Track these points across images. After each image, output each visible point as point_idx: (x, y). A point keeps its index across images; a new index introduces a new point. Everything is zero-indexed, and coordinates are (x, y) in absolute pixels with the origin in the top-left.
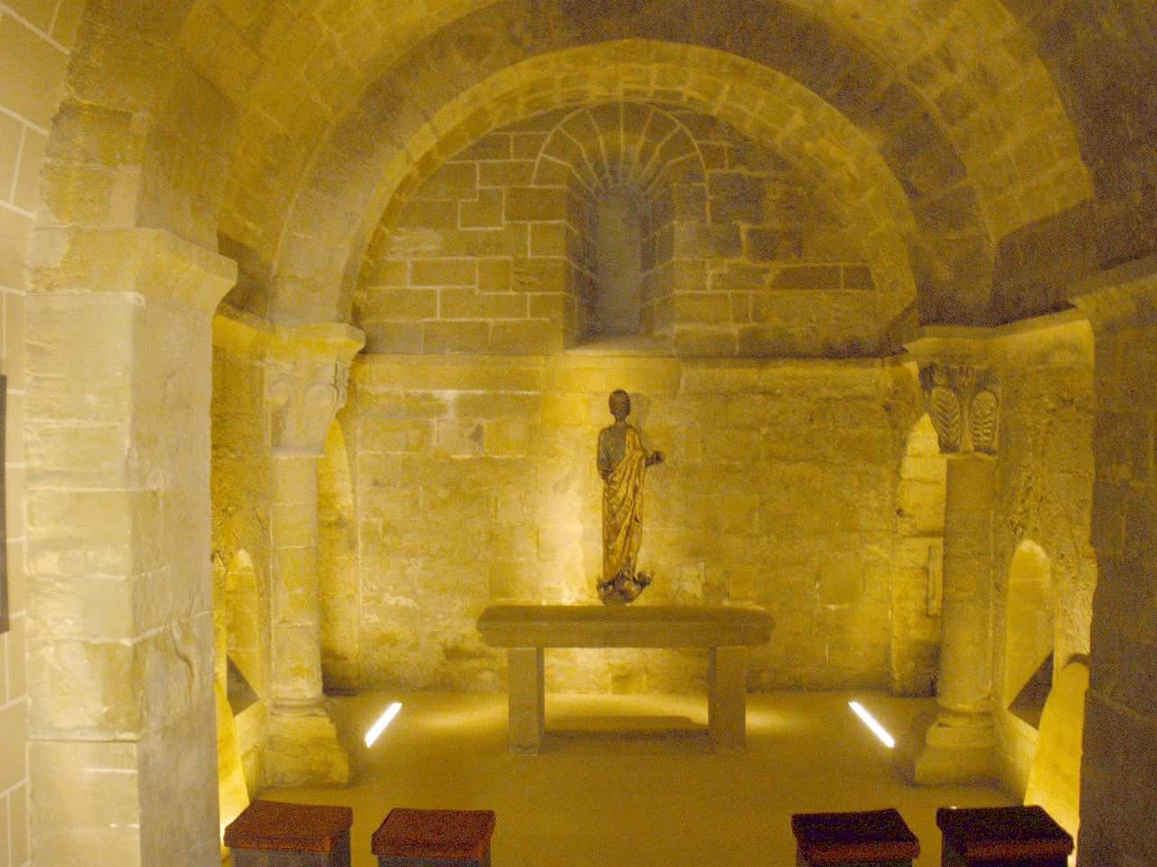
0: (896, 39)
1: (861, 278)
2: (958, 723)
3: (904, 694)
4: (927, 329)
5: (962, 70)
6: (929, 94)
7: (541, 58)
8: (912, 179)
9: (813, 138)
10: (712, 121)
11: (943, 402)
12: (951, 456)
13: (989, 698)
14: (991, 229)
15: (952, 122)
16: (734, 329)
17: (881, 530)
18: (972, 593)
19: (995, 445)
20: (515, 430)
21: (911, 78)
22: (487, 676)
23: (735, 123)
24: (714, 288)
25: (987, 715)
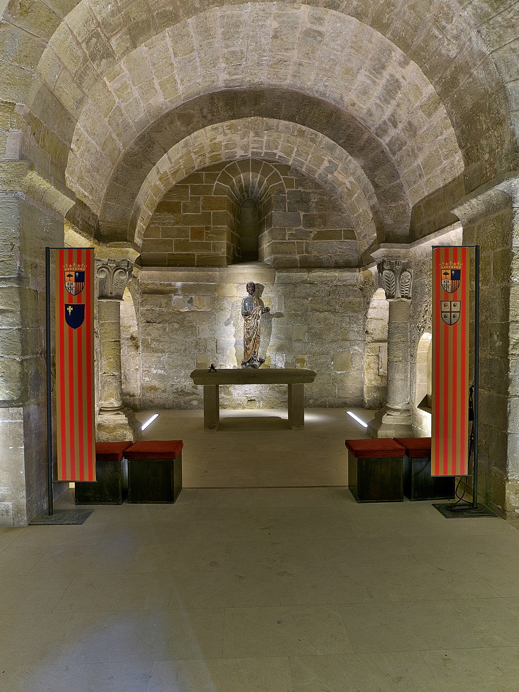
1: (351, 235)
2: (396, 414)
3: (370, 408)
4: (382, 245)
5: (400, 126)
6: (385, 141)
7: (215, 125)
8: (376, 179)
9: (332, 173)
10: (289, 167)
12: (391, 300)
13: (409, 403)
14: (411, 200)
15: (394, 154)
16: (298, 257)
17: (359, 340)
18: (401, 358)
19: (410, 295)
20: (206, 300)
21: (377, 134)
22: (195, 403)
23: (298, 168)
24: (289, 239)
25: (408, 411)
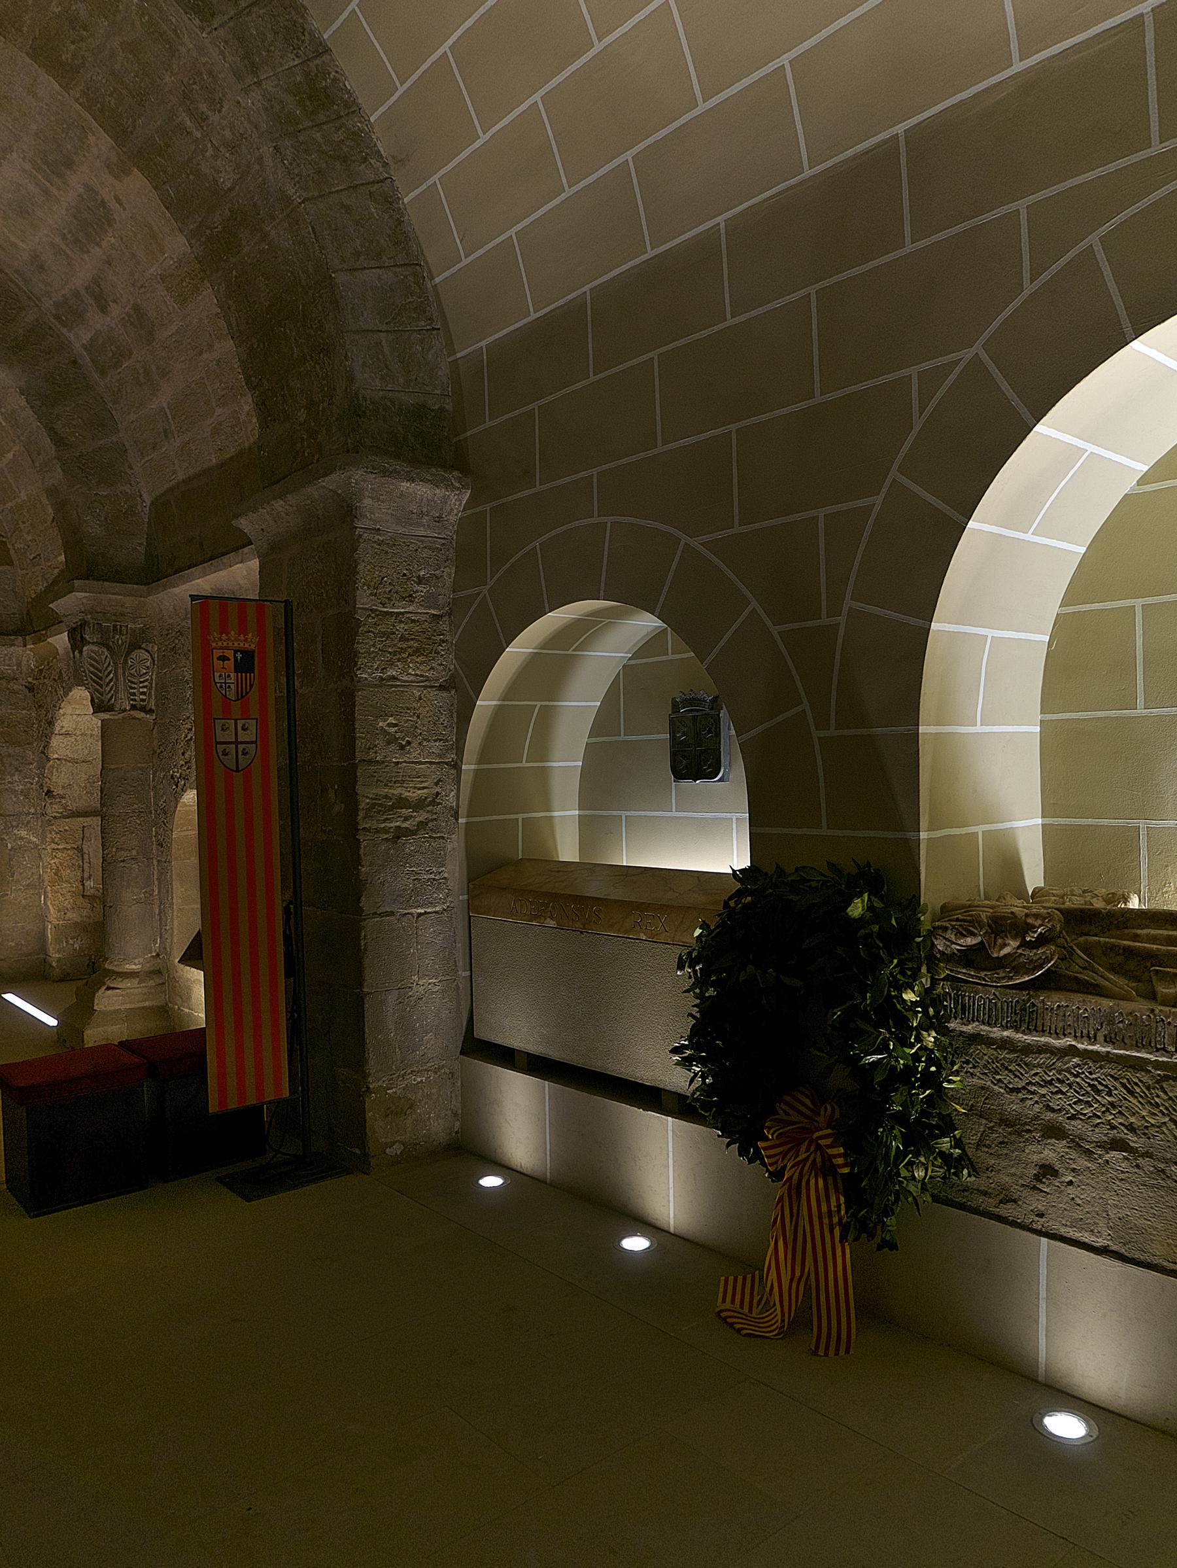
0: (42, 268)
3: (64, 979)
4: (77, 583)
5: (115, 311)
6: (79, 337)
8: (58, 426)
11: (97, 669)
12: (106, 716)
13: (158, 955)
15: (103, 372)
18: (134, 852)
19: (152, 704)
